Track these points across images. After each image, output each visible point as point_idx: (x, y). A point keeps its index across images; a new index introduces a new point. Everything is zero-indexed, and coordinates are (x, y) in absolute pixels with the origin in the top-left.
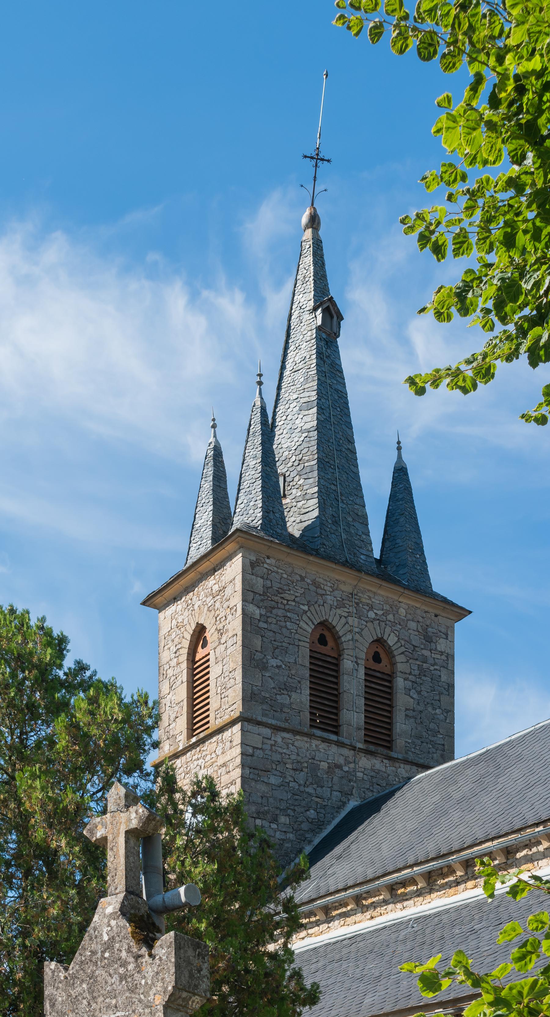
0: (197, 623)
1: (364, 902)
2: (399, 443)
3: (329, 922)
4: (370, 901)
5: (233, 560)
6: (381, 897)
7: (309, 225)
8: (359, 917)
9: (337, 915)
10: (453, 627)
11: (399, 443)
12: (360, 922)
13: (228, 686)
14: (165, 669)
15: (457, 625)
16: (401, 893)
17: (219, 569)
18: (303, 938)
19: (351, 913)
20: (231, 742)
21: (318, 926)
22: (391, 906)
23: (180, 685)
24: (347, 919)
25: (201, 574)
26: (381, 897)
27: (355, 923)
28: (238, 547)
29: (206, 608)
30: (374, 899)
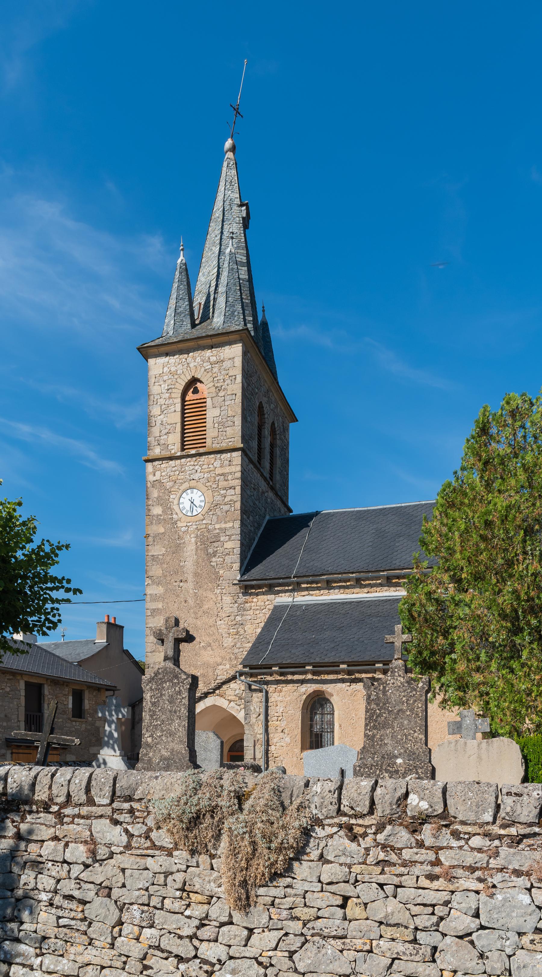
0: (193, 377)
1: (362, 582)
2: (263, 307)
3: (329, 590)
4: (367, 582)
5: (233, 346)
6: (380, 581)
7: (232, 150)
8: (357, 590)
9: (337, 586)
10: (288, 426)
11: (263, 307)
12: (358, 593)
13: (227, 425)
14: (156, 398)
15: (290, 424)
16: (395, 582)
17: (217, 348)
18: (304, 596)
19: (350, 587)
20: (230, 461)
21: (320, 590)
22: (386, 588)
23: (172, 412)
24: (346, 590)
25: (198, 345)
26: (380, 581)
27: (353, 593)
28: (239, 339)
29: (203, 369)
30: (371, 582)
